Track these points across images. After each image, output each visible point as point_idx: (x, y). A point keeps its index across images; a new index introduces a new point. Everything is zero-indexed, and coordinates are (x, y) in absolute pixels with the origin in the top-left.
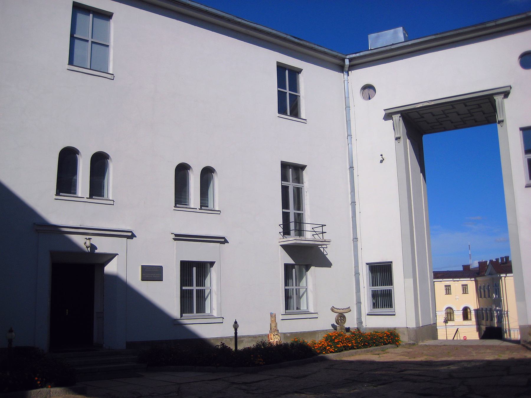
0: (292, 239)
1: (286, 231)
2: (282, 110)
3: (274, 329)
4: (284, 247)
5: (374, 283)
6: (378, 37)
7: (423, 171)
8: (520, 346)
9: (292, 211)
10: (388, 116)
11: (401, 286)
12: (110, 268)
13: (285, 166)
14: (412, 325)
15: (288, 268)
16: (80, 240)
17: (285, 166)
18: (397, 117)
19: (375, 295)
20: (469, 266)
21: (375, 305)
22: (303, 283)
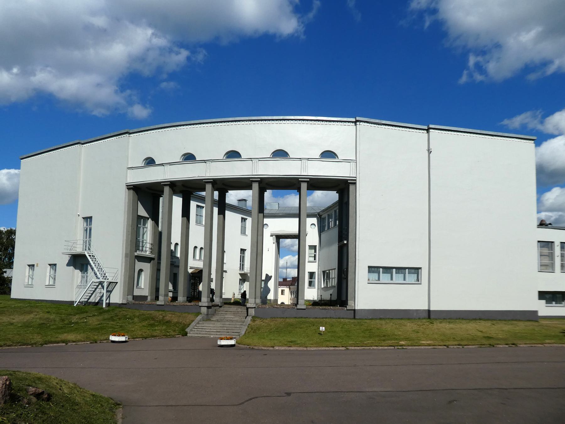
0: (243, 272)
2: (241, 233)
10: (272, 236)
13: (241, 250)
15: (240, 280)
17: (241, 250)
18: (274, 236)
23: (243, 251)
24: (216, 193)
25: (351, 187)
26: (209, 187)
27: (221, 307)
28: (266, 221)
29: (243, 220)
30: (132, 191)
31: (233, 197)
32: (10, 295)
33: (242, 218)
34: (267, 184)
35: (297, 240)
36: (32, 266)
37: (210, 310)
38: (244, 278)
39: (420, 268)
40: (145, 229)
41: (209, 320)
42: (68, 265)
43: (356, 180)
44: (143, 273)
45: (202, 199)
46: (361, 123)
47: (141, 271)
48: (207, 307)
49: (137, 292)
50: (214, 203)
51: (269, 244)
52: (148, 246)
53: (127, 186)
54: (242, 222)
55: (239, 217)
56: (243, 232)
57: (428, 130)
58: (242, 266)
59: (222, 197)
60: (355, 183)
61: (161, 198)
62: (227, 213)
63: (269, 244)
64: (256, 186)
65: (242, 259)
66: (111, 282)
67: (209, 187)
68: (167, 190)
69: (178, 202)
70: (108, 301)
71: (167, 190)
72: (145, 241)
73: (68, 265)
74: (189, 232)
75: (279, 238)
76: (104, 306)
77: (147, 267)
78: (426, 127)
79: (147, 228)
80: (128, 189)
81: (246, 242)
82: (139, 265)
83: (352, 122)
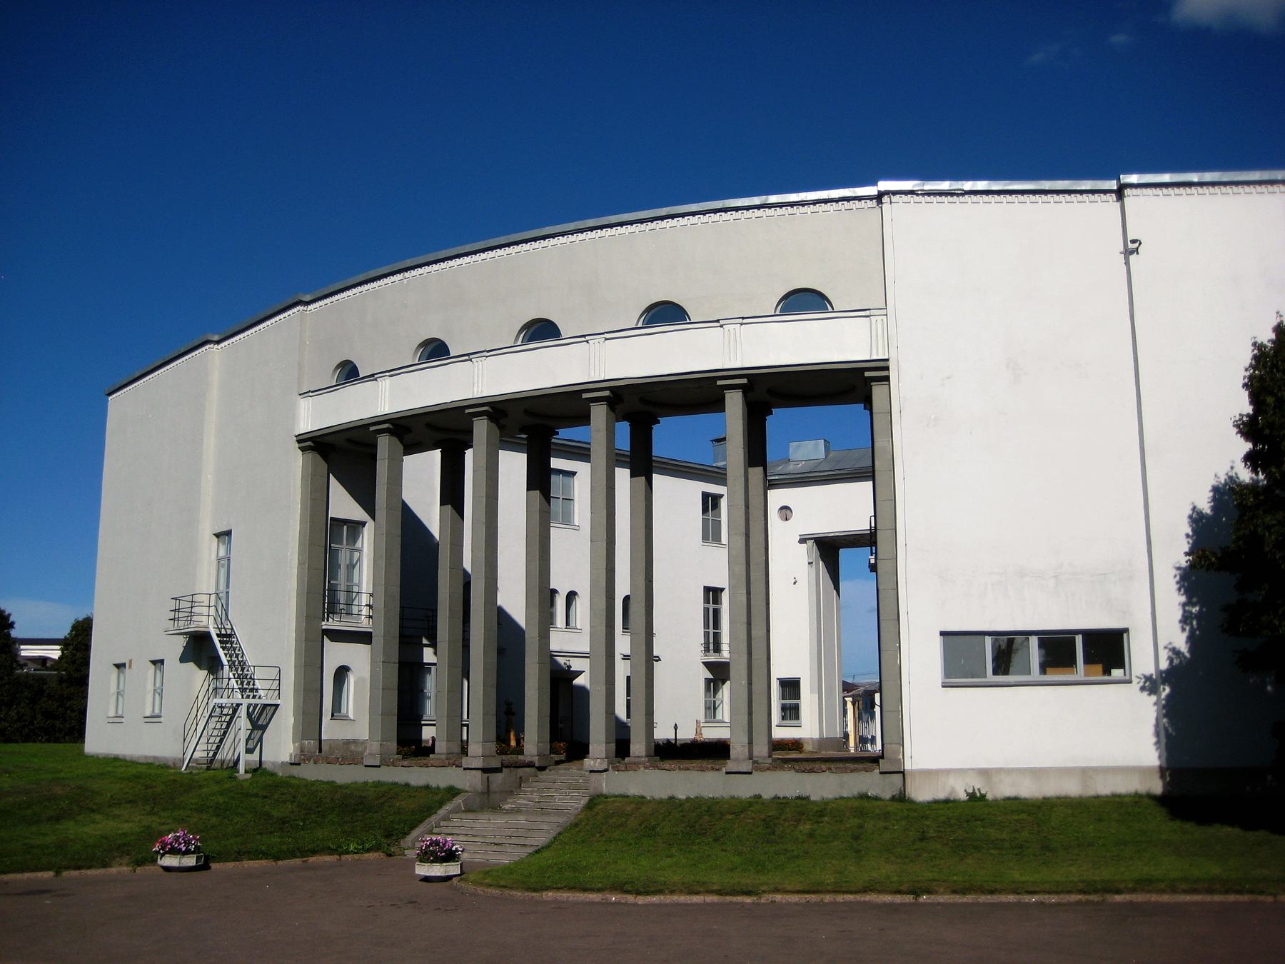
0: (713, 658)
1: (707, 650)
2: (705, 537)
3: (698, 732)
4: (706, 664)
5: (784, 697)
6: (798, 447)
7: (837, 587)
8: (533, 770)
9: (711, 630)
10: (803, 540)
11: (808, 701)
12: (579, 681)
13: (707, 590)
14: (816, 736)
15: (708, 681)
16: (561, 661)
17: (707, 590)
18: (810, 543)
19: (784, 708)
20: (1258, 346)
21: (783, 718)
22: (719, 695)
23: (713, 594)
24: (623, 429)
25: (877, 391)
26: (599, 413)
27: (542, 769)
28: (777, 498)
29: (711, 503)
30: (310, 455)
31: (670, 435)
32: (77, 732)
33: (705, 496)
34: (770, 391)
35: (843, 553)
36: (120, 666)
37: (493, 776)
38: (718, 674)
39: (1126, 630)
40: (356, 555)
41: (496, 808)
42: (183, 659)
43: (887, 369)
44: (351, 679)
45: (582, 453)
46: (895, 198)
47: (342, 672)
48: (485, 770)
49: (331, 731)
50: (616, 459)
51: (791, 566)
52: (365, 599)
53: (299, 442)
54: (705, 510)
55: (694, 490)
56: (710, 534)
57: (1120, 193)
58: (713, 643)
59: (641, 441)
60: (887, 379)
61: (469, 454)
62: (657, 479)
63: (791, 566)
64: (734, 401)
65: (712, 619)
66: (265, 706)
67: (599, 413)
68: (481, 428)
69: (513, 465)
70: (255, 757)
71: (481, 428)
72: (356, 589)
73: (183, 659)
74: (538, 552)
75: (829, 549)
76: (242, 770)
77: (358, 658)
78: (1113, 185)
79: (360, 550)
80: (303, 449)
81: (716, 566)
82: (336, 654)
83: (870, 198)
